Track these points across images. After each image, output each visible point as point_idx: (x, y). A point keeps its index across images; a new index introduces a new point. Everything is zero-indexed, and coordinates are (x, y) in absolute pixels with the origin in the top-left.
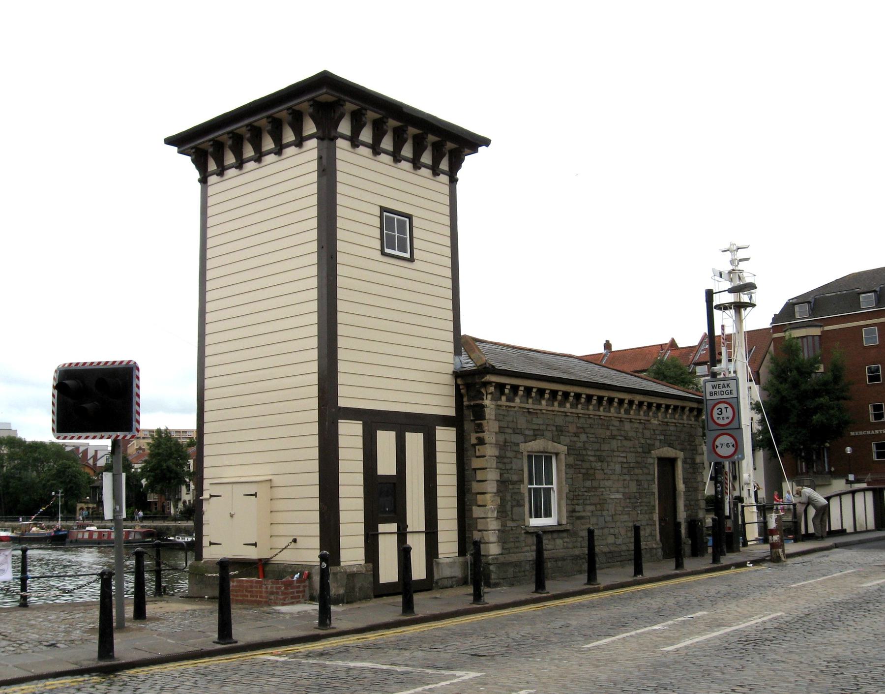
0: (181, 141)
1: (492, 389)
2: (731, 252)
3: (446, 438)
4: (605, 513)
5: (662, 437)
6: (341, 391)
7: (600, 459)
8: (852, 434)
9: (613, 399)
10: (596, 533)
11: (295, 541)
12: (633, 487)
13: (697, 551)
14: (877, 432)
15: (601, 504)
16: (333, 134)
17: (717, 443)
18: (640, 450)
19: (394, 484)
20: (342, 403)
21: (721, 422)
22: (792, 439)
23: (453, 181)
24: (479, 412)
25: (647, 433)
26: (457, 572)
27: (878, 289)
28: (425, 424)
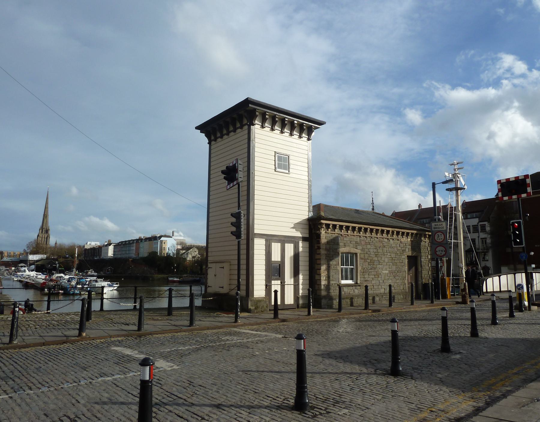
0: (202, 128)
6: (256, 226)
8: (536, 246)
13: (425, 298)
21: (438, 240)
22: (403, 257)
25: (402, 245)
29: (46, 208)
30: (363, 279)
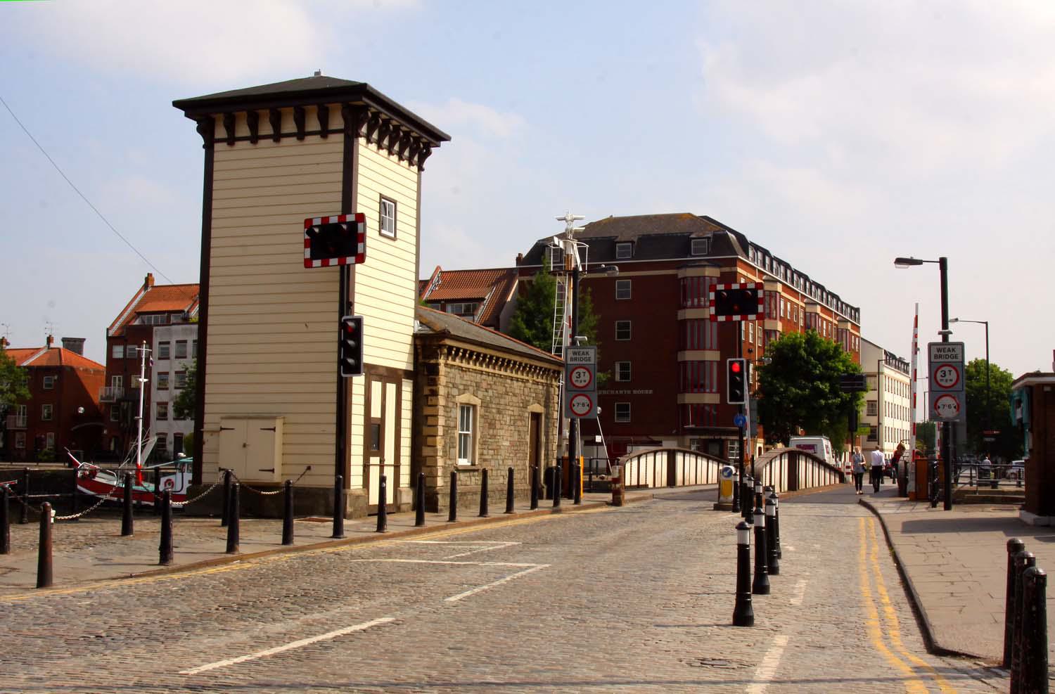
3: (407, 388)
4: (499, 457)
5: (534, 395)
7: (499, 412)
9: (493, 356)
10: (489, 473)
11: (309, 468)
12: (516, 437)
14: (621, 392)
15: (497, 450)
18: (521, 405)
19: (379, 425)
21: (577, 384)
23: (421, 169)
24: (434, 370)
27: (635, 240)
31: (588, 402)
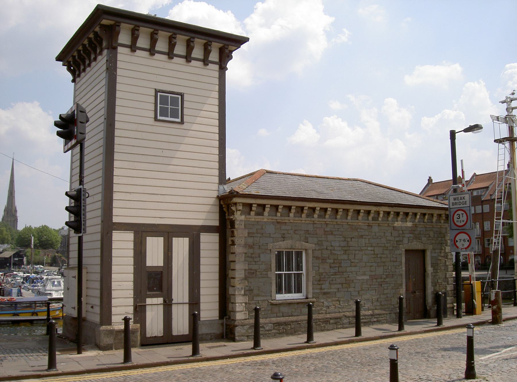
0: (58, 59)
1: (241, 208)
2: (507, 103)
6: (115, 212)
16: (114, 45)
17: (457, 239)
20: (115, 220)
22: (398, 252)
23: (223, 69)
26: (216, 330)
28: (193, 233)
29: (462, 170)
30: (318, 291)
31: (468, 239)
